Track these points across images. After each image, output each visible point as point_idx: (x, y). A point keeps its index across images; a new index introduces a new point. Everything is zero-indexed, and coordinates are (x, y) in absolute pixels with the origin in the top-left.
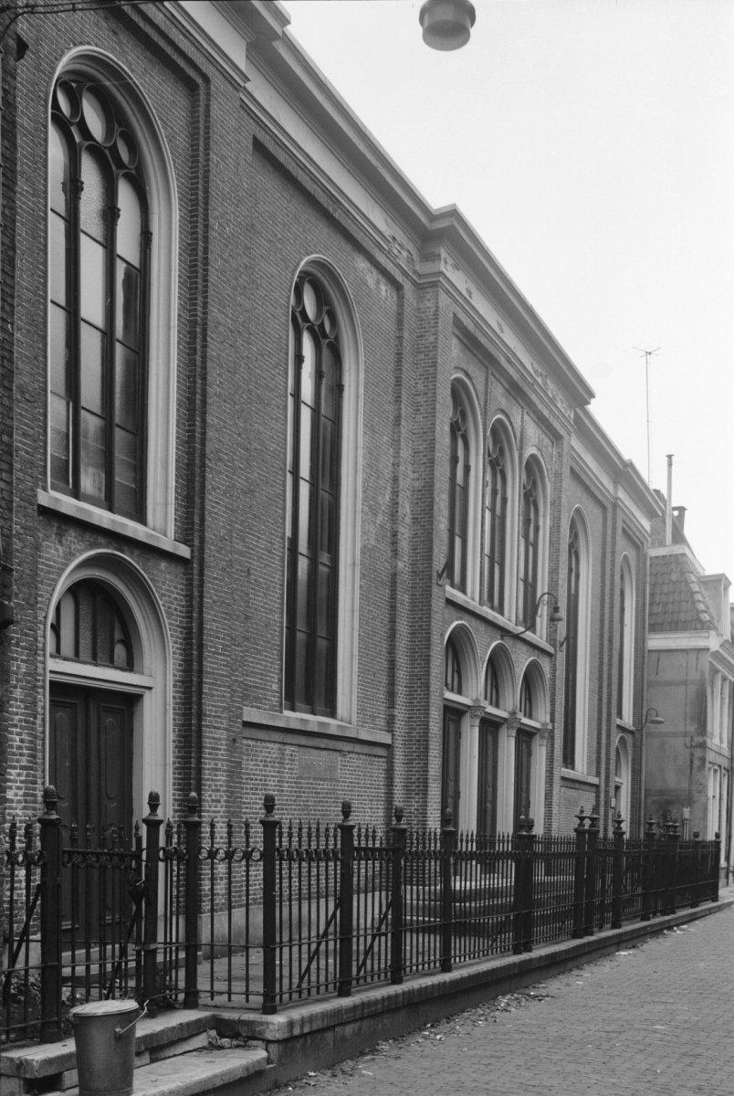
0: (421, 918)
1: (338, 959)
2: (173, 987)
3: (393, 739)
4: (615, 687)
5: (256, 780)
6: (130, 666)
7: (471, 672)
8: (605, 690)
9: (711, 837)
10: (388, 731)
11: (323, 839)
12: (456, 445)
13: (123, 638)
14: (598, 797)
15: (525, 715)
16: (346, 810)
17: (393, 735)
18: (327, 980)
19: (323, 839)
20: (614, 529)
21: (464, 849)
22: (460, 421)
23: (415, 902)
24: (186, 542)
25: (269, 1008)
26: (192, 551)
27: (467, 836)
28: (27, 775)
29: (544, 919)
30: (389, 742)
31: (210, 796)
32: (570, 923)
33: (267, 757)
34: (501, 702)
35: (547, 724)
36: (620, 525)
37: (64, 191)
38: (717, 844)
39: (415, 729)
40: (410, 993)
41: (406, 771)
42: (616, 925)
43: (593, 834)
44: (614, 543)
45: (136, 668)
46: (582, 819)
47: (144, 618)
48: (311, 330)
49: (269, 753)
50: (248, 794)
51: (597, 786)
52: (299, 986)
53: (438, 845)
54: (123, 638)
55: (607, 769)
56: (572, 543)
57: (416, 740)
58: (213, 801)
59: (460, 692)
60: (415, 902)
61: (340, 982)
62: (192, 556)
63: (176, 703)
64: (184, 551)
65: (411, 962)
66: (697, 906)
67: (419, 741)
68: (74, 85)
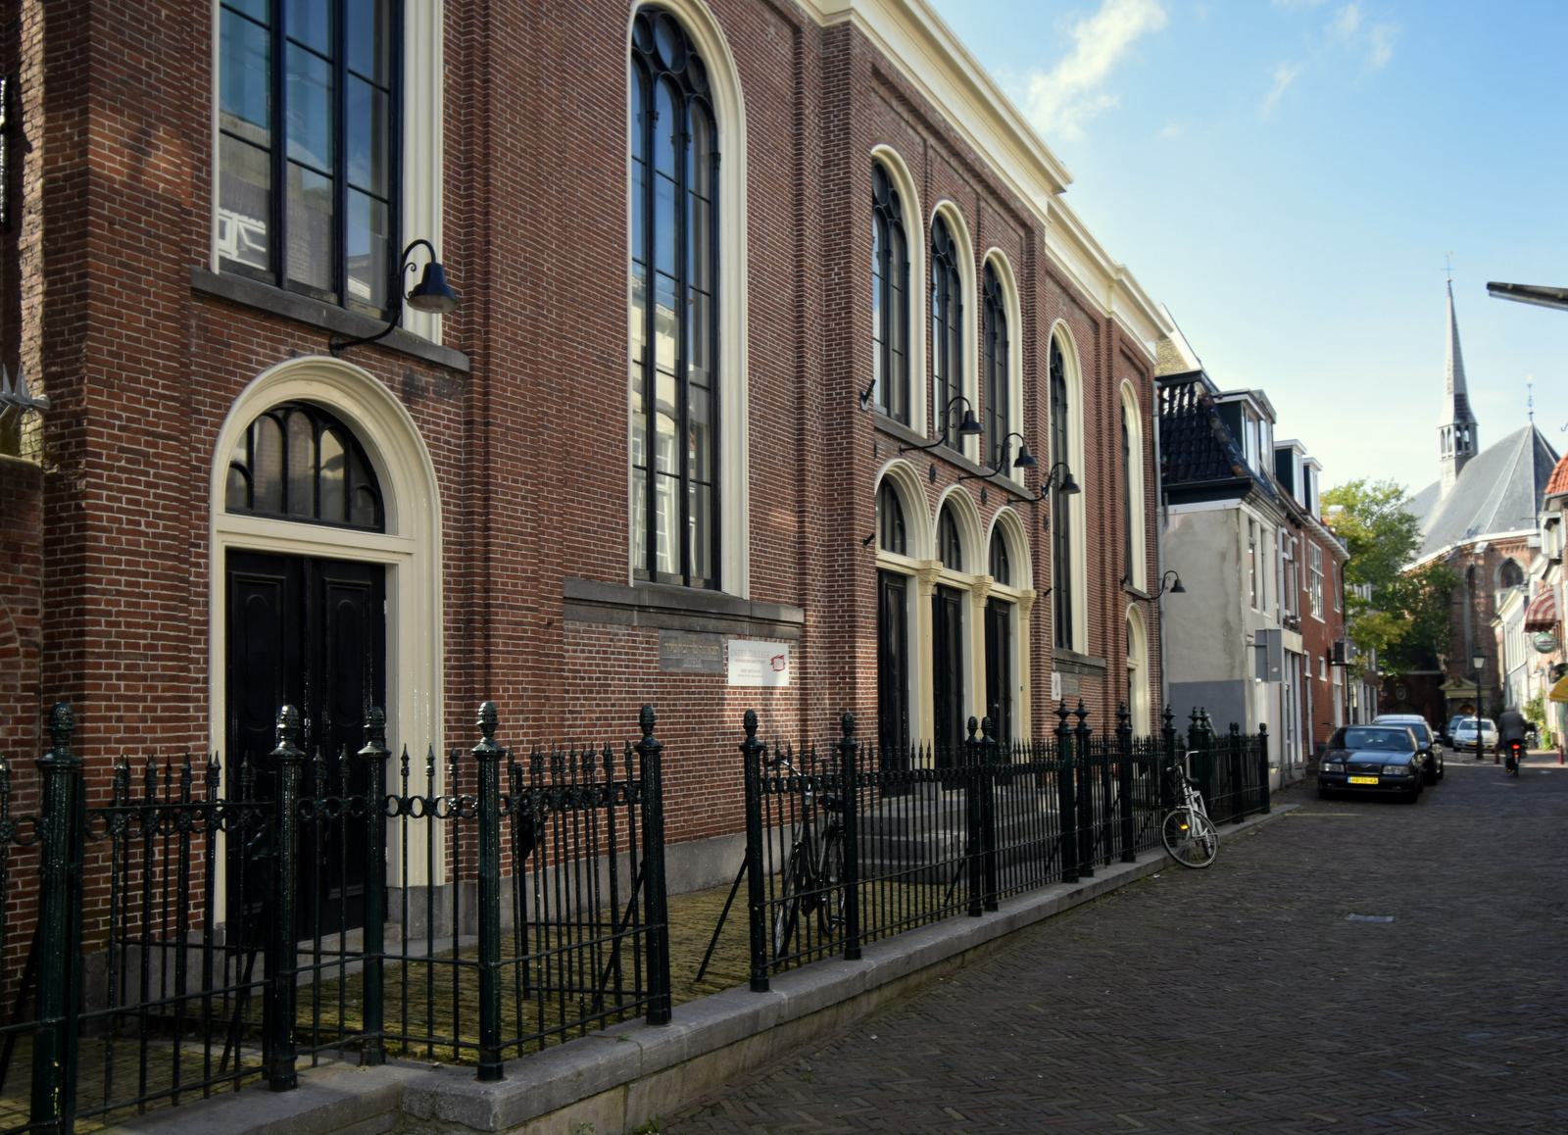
0: (895, 863)
1: (644, 967)
2: (576, 987)
3: (805, 616)
4: (1120, 535)
5: (590, 679)
6: (379, 525)
7: (918, 526)
8: (1108, 549)
9: (1252, 730)
10: (800, 606)
11: (925, 759)
12: (946, 280)
13: (369, 485)
14: (1105, 682)
15: (883, 547)
16: (647, 723)
17: (805, 610)
18: (883, 924)
19: (925, 759)
20: (1110, 349)
21: (917, 767)
22: (891, 206)
23: (886, 838)
24: (461, 349)
25: (490, 1071)
26: (472, 361)
27: (921, 749)
28: (515, 705)
29: (1018, 857)
30: (802, 621)
31: (506, 705)
32: (1057, 864)
33: (609, 646)
34: (908, 549)
35: (1029, 592)
36: (1116, 345)
37: (673, 142)
38: (1263, 738)
39: (837, 601)
40: (1011, 920)
41: (829, 658)
42: (1128, 857)
43: (1082, 732)
44: (1110, 367)
45: (387, 528)
46: (1195, 719)
47: (396, 452)
48: (670, 81)
49: (611, 640)
50: (578, 699)
51: (1104, 669)
52: (945, 905)
53: (932, 760)
54: (369, 485)
55: (1116, 646)
56: (1056, 367)
57: (839, 617)
58: (511, 712)
59: (903, 552)
60: (877, 837)
61: (847, 942)
62: (472, 368)
63: (449, 575)
64: (460, 362)
65: (883, 924)
66: (1242, 821)
67: (843, 617)
68: (1398, 605)
